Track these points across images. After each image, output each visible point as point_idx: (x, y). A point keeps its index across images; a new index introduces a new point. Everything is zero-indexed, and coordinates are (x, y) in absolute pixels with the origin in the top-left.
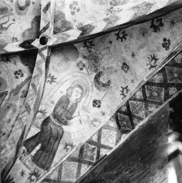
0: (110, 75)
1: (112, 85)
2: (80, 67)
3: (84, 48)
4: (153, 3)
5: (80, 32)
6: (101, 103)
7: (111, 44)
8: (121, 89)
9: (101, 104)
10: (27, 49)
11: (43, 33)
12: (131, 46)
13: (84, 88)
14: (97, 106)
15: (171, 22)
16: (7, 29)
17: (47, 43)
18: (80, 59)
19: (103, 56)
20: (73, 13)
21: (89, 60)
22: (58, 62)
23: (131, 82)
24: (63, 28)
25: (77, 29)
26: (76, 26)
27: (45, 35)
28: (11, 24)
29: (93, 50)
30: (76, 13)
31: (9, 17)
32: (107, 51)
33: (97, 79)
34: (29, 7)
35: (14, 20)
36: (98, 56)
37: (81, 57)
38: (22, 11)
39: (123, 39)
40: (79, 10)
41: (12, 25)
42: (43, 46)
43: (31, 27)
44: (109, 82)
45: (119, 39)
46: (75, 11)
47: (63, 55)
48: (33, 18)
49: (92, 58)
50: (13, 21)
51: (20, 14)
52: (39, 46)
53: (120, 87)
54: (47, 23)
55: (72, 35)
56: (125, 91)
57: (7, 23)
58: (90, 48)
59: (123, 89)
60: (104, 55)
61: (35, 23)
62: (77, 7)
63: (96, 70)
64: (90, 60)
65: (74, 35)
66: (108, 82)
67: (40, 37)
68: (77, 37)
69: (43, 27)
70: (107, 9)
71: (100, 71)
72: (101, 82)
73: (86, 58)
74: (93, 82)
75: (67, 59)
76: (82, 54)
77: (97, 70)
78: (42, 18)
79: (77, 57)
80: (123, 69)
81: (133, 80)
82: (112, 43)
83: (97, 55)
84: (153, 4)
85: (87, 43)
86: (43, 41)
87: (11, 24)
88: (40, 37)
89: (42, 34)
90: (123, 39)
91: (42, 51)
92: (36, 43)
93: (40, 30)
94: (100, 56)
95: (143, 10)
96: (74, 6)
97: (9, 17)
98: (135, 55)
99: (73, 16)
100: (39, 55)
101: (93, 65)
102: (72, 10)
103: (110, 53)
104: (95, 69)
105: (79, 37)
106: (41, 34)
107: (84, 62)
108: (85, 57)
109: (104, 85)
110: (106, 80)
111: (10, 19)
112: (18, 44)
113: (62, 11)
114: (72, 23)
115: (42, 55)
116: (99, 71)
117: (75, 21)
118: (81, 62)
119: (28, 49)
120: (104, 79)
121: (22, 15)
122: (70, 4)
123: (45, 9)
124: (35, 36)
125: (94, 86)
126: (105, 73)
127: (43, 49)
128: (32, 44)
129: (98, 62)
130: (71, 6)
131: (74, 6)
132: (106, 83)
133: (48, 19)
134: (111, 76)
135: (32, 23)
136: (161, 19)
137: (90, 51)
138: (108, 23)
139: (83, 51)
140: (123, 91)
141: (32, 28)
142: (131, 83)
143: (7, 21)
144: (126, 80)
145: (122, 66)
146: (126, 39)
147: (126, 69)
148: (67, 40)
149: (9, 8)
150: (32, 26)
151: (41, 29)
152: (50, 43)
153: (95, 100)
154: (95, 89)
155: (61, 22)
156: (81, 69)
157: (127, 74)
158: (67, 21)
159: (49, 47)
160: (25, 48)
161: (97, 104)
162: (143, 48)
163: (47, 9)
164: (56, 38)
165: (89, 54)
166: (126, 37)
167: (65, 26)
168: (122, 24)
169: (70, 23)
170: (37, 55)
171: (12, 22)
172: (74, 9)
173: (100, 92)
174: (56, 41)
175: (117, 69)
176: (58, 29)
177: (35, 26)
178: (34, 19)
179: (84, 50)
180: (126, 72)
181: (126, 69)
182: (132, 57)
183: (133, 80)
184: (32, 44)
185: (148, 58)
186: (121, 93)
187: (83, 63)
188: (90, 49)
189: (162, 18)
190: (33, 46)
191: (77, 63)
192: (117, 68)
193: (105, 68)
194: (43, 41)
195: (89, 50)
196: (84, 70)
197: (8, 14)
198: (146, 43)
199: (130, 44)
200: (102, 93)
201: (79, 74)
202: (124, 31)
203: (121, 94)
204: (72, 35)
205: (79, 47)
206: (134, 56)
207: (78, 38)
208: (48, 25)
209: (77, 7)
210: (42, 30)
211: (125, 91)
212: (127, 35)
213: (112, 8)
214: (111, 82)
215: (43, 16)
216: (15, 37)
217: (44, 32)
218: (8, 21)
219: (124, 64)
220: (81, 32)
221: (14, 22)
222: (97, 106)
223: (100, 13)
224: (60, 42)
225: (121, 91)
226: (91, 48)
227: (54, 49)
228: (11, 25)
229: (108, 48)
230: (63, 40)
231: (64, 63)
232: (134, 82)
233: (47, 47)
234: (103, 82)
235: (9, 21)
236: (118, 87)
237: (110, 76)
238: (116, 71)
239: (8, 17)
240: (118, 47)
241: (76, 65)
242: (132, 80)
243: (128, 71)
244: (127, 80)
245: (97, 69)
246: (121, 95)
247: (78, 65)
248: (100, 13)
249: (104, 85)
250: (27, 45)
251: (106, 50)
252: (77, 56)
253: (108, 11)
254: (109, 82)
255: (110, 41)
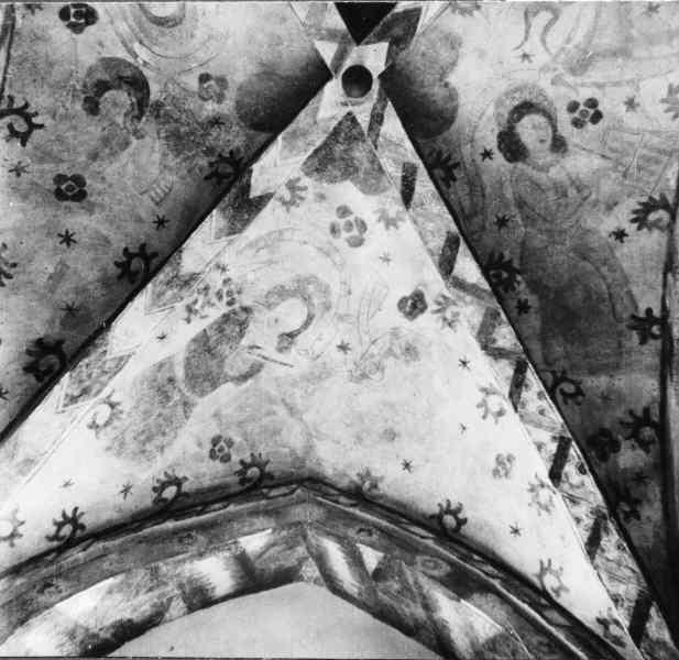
0: (106, 132)
1: (78, 106)
2: (212, 82)
3: (231, 148)
4: (66, 409)
5: (255, 193)
6: (68, 26)
7: (156, 219)
8: (35, 120)
9: (67, 23)
10: (389, 16)
11: (375, 101)
12: (91, 255)
13: (155, 30)
14: (73, 11)
15: (6, 393)
16: (526, 14)
17: (340, 86)
18: (227, 107)
19: (165, 167)
20: (344, 211)
21: (199, 124)
22: (286, 44)
23: (23, 165)
24: (345, 151)
25: (272, 191)
26: (305, 188)
27: (362, 103)
28: (526, 39)
29: (203, 162)
30: (334, 218)
31: (550, 54)
32: (158, 191)
33: (138, 84)
34: (497, 132)
35: (525, 56)
36: (177, 156)
37: (226, 112)
38: (516, 103)
39: (124, 259)
40: (334, 230)
41: (522, 38)
42: (348, 63)
43: (447, 80)
44: (93, 107)
45: (136, 251)
46: (342, 222)
47: (288, 77)
48: (460, 111)
49: (192, 138)
50: (527, 52)
51: (517, 90)
52: (360, 57)
53: (47, 124)
54: (381, 139)
55: (275, 166)
56: (21, 126)
57: (541, 30)
58: (216, 162)
59: (32, 127)
60: (161, 172)
61: (440, 103)
62: (344, 235)
63: (158, 111)
64: (195, 125)
65: (276, 167)
66: (97, 104)
67: (376, 86)
68: (255, 174)
69: (385, 120)
70: (245, 291)
71: (144, 119)
72: (119, 87)
73: (209, 122)
74: (141, 68)
75: (268, 72)
76: (228, 124)
77: (155, 113)
78: (408, 144)
79: (239, 105)
80: (74, 181)
81: (18, 175)
82: (155, 222)
83: (182, 156)
84: (65, 405)
85: (229, 170)
86: (357, 80)
87: (526, 39)
88: (376, 86)
89: (375, 96)
90: (124, 259)
91: (339, 47)
92: (374, 57)
93: (390, 103)
94: (172, 161)
95: (90, 376)
96: (355, 232)
97: (550, 54)
98: (61, 243)
99: (337, 205)
100: (338, 28)
101: (176, 121)
102: (351, 218)
103: (144, 192)
104: (162, 112)
105: (250, 177)
106: (380, 94)
107: (210, 108)
108: (216, 121)
109: (102, 87)
110: (109, 106)
111: (542, 49)
112: (427, 10)
113: (377, 197)
114: (325, 185)
115: (332, 35)
116: (148, 114)
117: (322, 197)
118: (220, 98)
119: (385, 19)
120: (115, 104)
121: (507, 94)
122: (369, 227)
123: (412, 175)
124: (412, 67)
125: (130, 60)
126: (125, 123)
127: (341, 56)
128: (384, 46)
129: (167, 138)
130: (363, 226)
131: (355, 232)
132: (102, 99)
133: (387, 153)
134: (100, 129)
135: (452, 96)
136: (39, 379)
137: (210, 151)
138: (176, 276)
139: (231, 138)
140: (28, 118)
141: (441, 80)
142: (20, 163)
143: (549, 39)
144: (44, 156)
145: (84, 184)
146: (117, 264)
147: (63, 187)
148: (284, 139)
149: (570, 79)
150: (446, 85)
151: (388, 109)
152: (333, 90)
153: (93, 23)
154: (121, 54)
155: (361, 164)
156: (204, 78)
157: (50, 177)
158: (345, 179)
159: (328, 77)
160: (397, 14)
161: (77, 15)
162: (50, 277)
163: (404, 178)
164: (323, 120)
165: (207, 144)
166: (119, 271)
167: (342, 162)
168: (130, 304)
169: (333, 180)
170: (346, 23)
171: (527, 48)
172: (349, 226)
173: (100, 57)
174: (316, 110)
175: (95, 164)
176: (355, 139)
177: (433, 96)
178: (455, 109)
179: (229, 141)
180: (60, 179)
181: (63, 187)
182: (67, 232)
183: (18, 175)
184: (384, 46)
185: (14, 265)
186: (30, 110)
187: (210, 102)
188: (213, 160)
189: (40, 385)
190: (380, 38)
191: (230, 84)
192: (95, 166)
193: (138, 138)
194: (357, 80)
195: (213, 155)
196: (192, 82)
197: (559, 60)
198: (50, 295)
199: (95, 260)
200: (89, 59)
201: (202, 55)
202: (132, 282)
203: (27, 105)
204: (275, 166)
205: (250, 138)
206: (61, 239)
207: (251, 171)
208: (374, 137)
209: (344, 235)
210: (384, 108)
211: (21, 126)
212: (120, 277)
213: (230, 304)
214: (84, 112)
215: (406, 150)
216: (476, 13)
217: (374, 108)
218: (543, 41)
219: (80, 196)
220: (251, 197)
221: (520, 52)
222: (73, 11)
223: (260, 268)
224: (303, 119)
225: (36, 114)
226: (211, 164)
227: (316, 75)
228: (523, 34)
229: (161, 201)
230: (294, 132)
231: (266, 55)
232: (11, 171)
233: (336, 72)
234: (111, 92)
235: (539, 44)
236: (54, 117)
237: (104, 129)
238: (94, 156)
239: (553, 51)
240: (131, 227)
241: (228, 78)
242: (22, 174)
243: (55, 187)
244: (41, 160)
245: (158, 116)
246: (23, 103)
247: (222, 81)
248: (260, 268)
249: (102, 87)
250: (398, 31)
251: (163, 191)
252: (242, 108)
253: (235, 290)
254: (93, 107)
255: (166, 225)
